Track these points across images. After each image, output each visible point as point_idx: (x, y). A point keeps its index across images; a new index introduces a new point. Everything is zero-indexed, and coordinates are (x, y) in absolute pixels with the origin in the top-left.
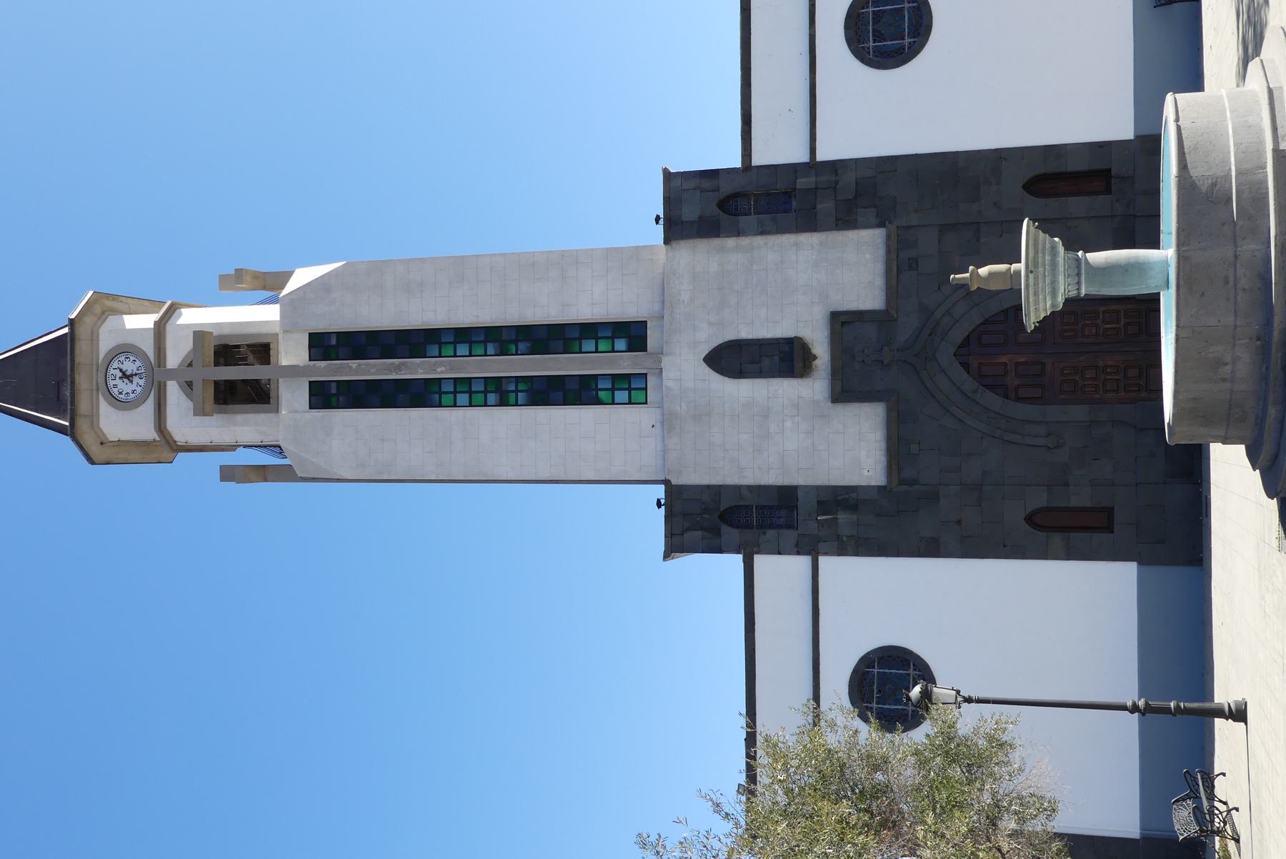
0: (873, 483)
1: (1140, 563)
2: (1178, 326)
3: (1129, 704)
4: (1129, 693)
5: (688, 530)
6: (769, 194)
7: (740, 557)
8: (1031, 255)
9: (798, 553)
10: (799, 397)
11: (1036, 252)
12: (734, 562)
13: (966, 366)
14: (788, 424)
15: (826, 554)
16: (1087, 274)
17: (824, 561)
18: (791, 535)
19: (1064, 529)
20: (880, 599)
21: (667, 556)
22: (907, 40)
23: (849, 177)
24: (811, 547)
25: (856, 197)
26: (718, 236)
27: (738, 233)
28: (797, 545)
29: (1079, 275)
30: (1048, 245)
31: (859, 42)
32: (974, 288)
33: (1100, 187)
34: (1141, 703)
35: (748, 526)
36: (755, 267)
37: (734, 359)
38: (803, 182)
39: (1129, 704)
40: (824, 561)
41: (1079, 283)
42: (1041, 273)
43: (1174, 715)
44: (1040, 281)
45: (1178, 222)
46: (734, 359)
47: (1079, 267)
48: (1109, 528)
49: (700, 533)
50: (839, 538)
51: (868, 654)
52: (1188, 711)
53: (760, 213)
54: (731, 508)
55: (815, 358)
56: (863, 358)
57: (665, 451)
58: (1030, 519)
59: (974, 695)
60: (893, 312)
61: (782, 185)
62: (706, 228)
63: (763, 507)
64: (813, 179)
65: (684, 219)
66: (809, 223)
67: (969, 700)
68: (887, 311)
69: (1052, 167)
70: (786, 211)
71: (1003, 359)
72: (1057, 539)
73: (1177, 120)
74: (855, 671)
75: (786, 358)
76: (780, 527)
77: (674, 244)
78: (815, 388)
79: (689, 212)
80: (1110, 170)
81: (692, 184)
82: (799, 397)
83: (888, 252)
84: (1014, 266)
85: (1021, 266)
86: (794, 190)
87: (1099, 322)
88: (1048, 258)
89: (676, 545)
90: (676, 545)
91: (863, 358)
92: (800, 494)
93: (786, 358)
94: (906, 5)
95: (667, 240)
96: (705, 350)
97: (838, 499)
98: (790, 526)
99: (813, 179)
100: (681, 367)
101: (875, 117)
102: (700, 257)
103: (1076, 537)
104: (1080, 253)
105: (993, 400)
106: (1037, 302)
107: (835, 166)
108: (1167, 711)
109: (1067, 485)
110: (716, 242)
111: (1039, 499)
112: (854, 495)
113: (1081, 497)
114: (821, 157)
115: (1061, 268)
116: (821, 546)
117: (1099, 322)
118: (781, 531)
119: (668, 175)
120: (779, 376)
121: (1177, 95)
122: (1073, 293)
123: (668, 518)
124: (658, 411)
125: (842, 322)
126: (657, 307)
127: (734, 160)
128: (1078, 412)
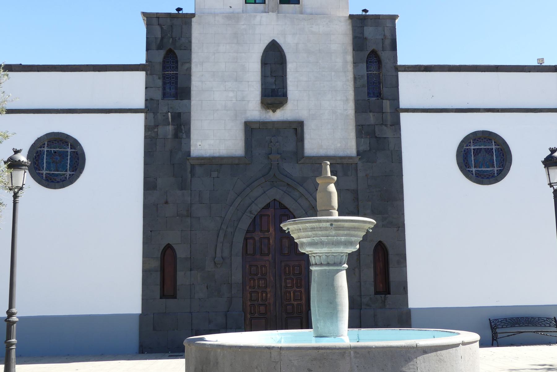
0: (192, 148)
1: (140, 315)
2: (281, 348)
3: (14, 310)
4: (22, 310)
5: (162, 28)
6: (380, 83)
7: (144, 62)
8: (346, 224)
9: (146, 100)
10: (248, 101)
11: (349, 229)
12: (141, 59)
13: (268, 206)
14: (231, 94)
15: (146, 118)
16: (329, 271)
17: (141, 117)
18: (158, 94)
19: (163, 268)
20: (116, 153)
21: (144, 14)
22: (474, 169)
23: (389, 133)
24: (150, 108)
25: (376, 137)
26: (354, 50)
27: (355, 63)
28: (152, 99)
29: (328, 264)
30: (353, 239)
31: (474, 140)
32: (319, 181)
33: (380, 288)
34: (14, 319)
35: (164, 68)
36: (333, 73)
37: (274, 60)
38: (387, 104)
39: (14, 310)
40: (141, 117)
41: (321, 265)
42: (327, 236)
43: (6, 342)
44: (324, 232)
45: (377, 348)
46: (274, 60)
47: (335, 264)
48: (163, 296)
49: (159, 36)
50: (157, 126)
51: (80, 145)
52: (8, 351)
53: (368, 77)
54: (176, 57)
55: (274, 111)
56: (274, 145)
57: (215, 15)
58: (169, 247)
59: (19, 200)
60: (302, 161)
61: (385, 91)
62: (359, 42)
63: (177, 78)
64: (389, 111)
65: (365, 28)
66: (361, 108)
67: (15, 196)
68: (303, 157)
69: (392, 258)
70: (369, 94)
71: (271, 230)
72: (156, 264)
73: (464, 344)
74: (68, 136)
75: (274, 92)
76: (164, 89)
77: (350, 21)
78: (255, 111)
79: (369, 32)
80: (389, 293)
81: (388, 34)
82: (248, 101)
83: (341, 158)
84: (336, 213)
85: (336, 215)
86: (382, 99)
87: (295, 288)
88: (343, 239)
89: (152, 20)
90: (152, 20)
91: (274, 145)
92: (185, 102)
93: (274, 92)
94: (496, 169)
95: (351, 17)
96: (280, 41)
97: (181, 125)
98: (164, 95)
99: (389, 111)
100: (269, 26)
101: (427, 151)
102: (341, 37)
103: (157, 277)
104: (346, 266)
105: (245, 223)
106: (305, 230)
107: (396, 125)
108: (9, 336)
109: (191, 270)
110: (350, 48)
111: (181, 252)
112: (184, 136)
113: (183, 278)
114: (403, 116)
115: (334, 250)
116: (151, 115)
117: (295, 288)
118: (161, 89)
119: (393, 18)
120: (262, 89)
121: (478, 343)
122: (312, 260)
123: (169, 15)
124: (241, 10)
125: (297, 128)
126: (309, 11)
127: (401, 61)
128: (237, 276)
